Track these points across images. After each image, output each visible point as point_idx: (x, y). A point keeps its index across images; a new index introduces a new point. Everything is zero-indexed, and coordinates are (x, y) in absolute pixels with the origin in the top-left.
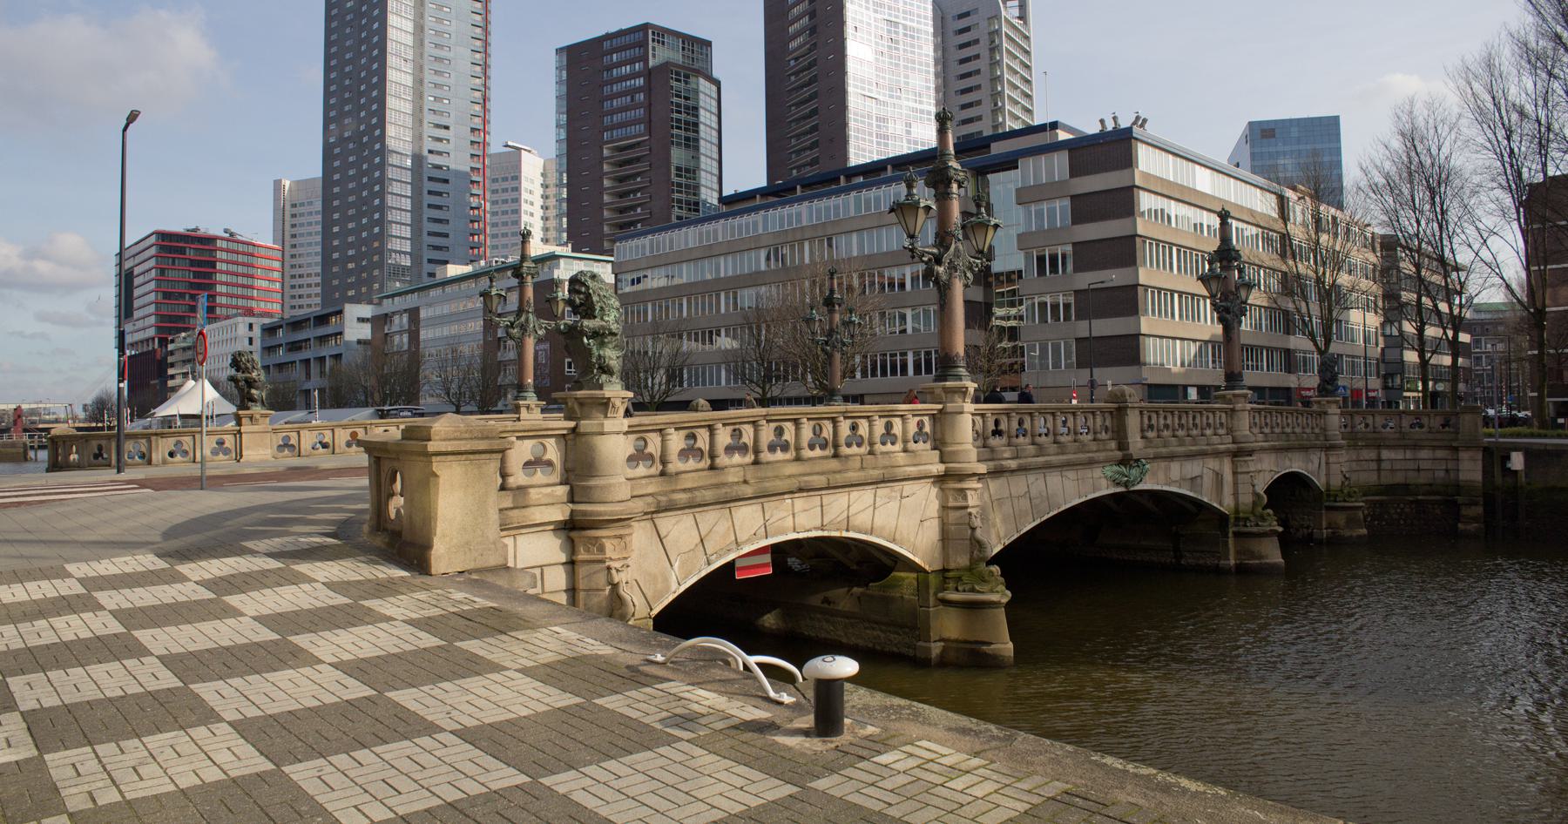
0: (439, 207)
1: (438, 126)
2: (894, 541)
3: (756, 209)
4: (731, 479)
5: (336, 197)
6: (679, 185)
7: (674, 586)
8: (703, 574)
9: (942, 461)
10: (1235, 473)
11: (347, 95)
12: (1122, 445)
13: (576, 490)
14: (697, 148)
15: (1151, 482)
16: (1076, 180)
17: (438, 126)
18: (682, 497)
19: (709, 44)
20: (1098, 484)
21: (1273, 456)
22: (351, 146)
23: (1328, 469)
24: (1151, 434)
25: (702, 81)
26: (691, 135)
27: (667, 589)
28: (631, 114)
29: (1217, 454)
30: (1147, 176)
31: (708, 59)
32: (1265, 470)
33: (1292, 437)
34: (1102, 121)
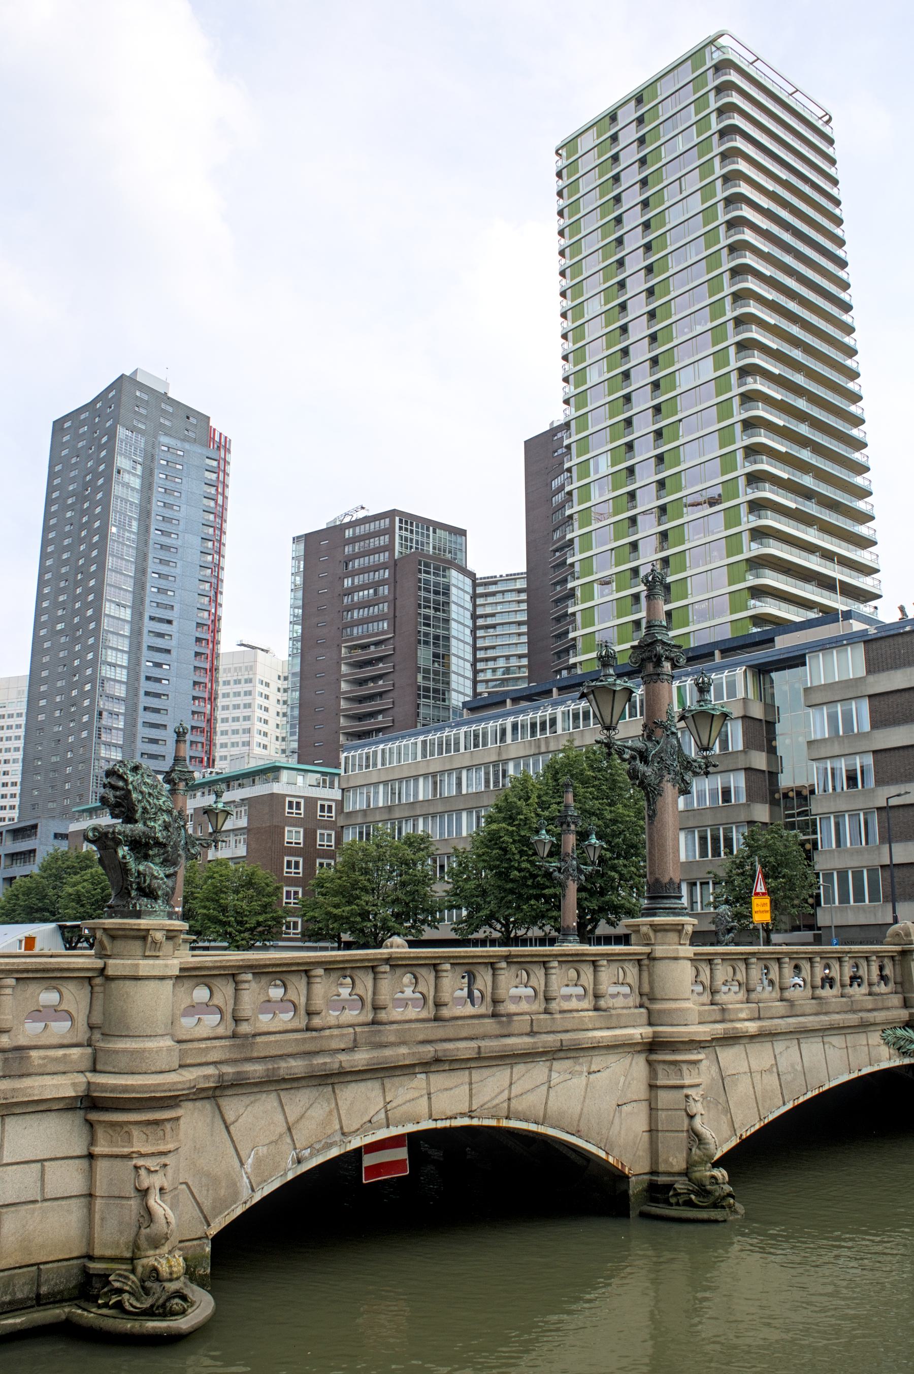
0: (157, 711)
2: (577, 1133)
6: (427, 689)
7: (245, 1193)
8: (290, 1176)
9: (650, 1024)
13: (100, 1055)
16: (871, 679)
18: (256, 1069)
25: (454, 573)
27: (235, 1197)
34: (902, 609)
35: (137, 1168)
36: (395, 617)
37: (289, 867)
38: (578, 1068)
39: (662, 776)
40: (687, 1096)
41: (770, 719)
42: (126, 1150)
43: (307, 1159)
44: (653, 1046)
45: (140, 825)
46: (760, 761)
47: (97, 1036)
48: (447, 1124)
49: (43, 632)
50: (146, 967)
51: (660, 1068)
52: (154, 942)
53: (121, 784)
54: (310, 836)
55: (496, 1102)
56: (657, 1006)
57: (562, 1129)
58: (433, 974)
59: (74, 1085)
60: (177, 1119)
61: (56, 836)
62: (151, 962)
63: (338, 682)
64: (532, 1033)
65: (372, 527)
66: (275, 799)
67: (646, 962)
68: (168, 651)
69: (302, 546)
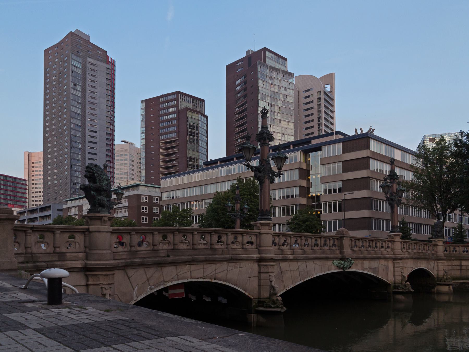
1: (92, 131)
3: (218, 167)
4: (161, 255)
5: (49, 159)
8: (148, 293)
9: (259, 254)
10: (394, 267)
11: (53, 116)
12: (342, 252)
14: (198, 143)
15: (357, 268)
16: (345, 155)
17: (92, 131)
19: (203, 101)
20: (331, 268)
21: (412, 261)
22: (55, 138)
23: (438, 268)
24: (355, 249)
25: (200, 116)
26: (195, 138)
28: (171, 129)
29: (385, 259)
30: (373, 153)
31: (203, 107)
32: (410, 267)
33: (421, 254)
34: (356, 131)
35: (102, 288)
36: (179, 132)
37: (143, 220)
38: (236, 266)
39: (265, 177)
40: (270, 275)
41: (308, 169)
42: (98, 283)
43: (154, 289)
44: (260, 260)
45: (98, 184)
46: (304, 183)
47: (87, 250)
48: (196, 280)
49: (47, 135)
50: (102, 228)
51: (262, 267)
52: (105, 221)
53: (91, 171)
54: (150, 209)
55: (211, 274)
56: (262, 248)
57: (232, 284)
58: (192, 235)
59: (81, 263)
60: (114, 274)
61: (58, 210)
62: (103, 227)
63: (159, 161)
64: (222, 254)
65: (170, 98)
66: (139, 196)
67: (258, 235)
68: (96, 143)
69: (144, 104)
